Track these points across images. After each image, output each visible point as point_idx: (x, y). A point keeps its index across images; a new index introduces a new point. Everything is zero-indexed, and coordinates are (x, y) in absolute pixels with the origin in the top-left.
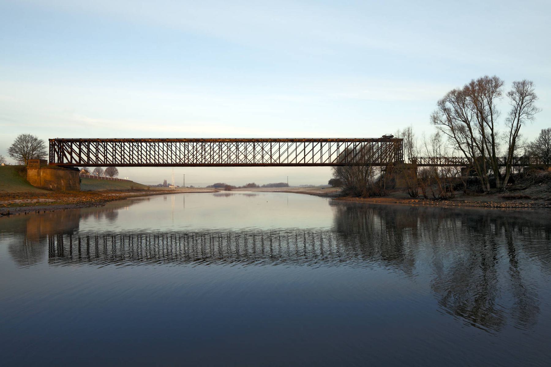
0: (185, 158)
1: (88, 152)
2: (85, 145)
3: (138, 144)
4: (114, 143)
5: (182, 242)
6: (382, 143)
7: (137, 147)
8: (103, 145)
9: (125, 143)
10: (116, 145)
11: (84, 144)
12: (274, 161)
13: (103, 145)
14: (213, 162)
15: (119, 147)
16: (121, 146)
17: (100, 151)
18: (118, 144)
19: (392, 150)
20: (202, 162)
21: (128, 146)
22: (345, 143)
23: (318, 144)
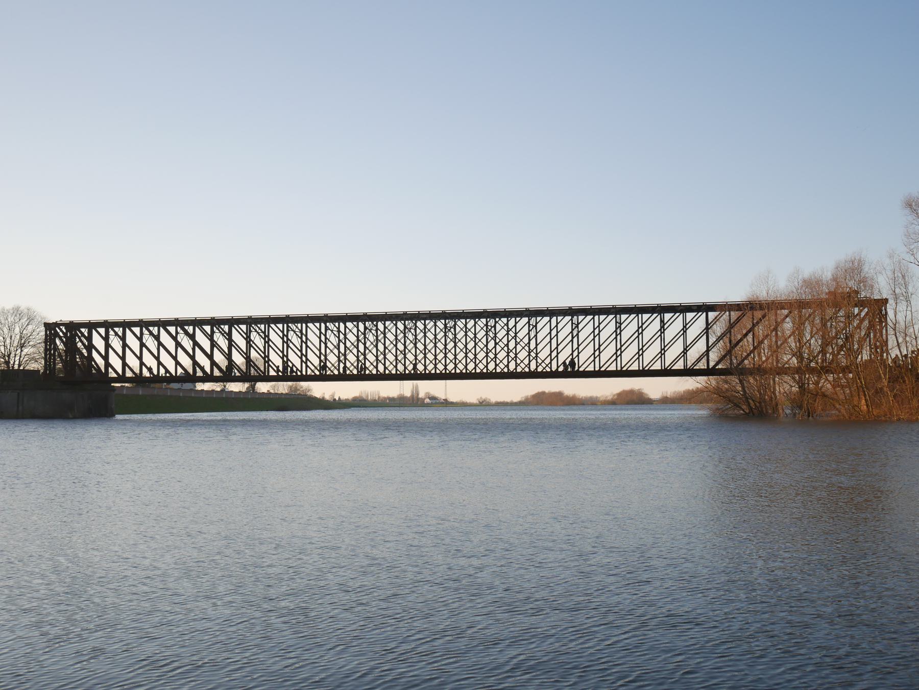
0: (437, 360)
1: (265, 347)
2: (259, 331)
3: (377, 326)
4: (323, 325)
5: (46, 663)
6: (711, 319)
7: (335, 333)
8: (297, 330)
9: (308, 324)
10: (327, 328)
11: (257, 329)
12: (482, 369)
13: (297, 330)
14: (537, 367)
15: (297, 335)
16: (339, 331)
17: (291, 345)
18: (333, 326)
19: (831, 327)
20: (529, 368)
21: (355, 330)
22: (682, 314)
23: (629, 316)
